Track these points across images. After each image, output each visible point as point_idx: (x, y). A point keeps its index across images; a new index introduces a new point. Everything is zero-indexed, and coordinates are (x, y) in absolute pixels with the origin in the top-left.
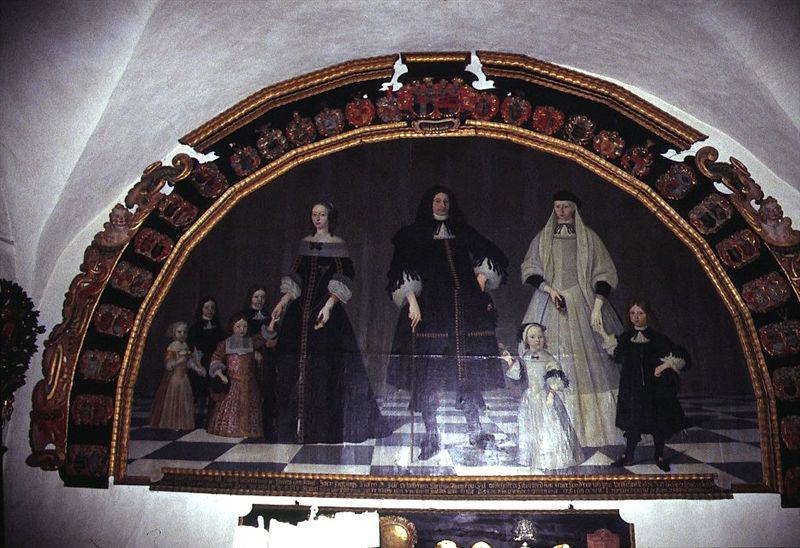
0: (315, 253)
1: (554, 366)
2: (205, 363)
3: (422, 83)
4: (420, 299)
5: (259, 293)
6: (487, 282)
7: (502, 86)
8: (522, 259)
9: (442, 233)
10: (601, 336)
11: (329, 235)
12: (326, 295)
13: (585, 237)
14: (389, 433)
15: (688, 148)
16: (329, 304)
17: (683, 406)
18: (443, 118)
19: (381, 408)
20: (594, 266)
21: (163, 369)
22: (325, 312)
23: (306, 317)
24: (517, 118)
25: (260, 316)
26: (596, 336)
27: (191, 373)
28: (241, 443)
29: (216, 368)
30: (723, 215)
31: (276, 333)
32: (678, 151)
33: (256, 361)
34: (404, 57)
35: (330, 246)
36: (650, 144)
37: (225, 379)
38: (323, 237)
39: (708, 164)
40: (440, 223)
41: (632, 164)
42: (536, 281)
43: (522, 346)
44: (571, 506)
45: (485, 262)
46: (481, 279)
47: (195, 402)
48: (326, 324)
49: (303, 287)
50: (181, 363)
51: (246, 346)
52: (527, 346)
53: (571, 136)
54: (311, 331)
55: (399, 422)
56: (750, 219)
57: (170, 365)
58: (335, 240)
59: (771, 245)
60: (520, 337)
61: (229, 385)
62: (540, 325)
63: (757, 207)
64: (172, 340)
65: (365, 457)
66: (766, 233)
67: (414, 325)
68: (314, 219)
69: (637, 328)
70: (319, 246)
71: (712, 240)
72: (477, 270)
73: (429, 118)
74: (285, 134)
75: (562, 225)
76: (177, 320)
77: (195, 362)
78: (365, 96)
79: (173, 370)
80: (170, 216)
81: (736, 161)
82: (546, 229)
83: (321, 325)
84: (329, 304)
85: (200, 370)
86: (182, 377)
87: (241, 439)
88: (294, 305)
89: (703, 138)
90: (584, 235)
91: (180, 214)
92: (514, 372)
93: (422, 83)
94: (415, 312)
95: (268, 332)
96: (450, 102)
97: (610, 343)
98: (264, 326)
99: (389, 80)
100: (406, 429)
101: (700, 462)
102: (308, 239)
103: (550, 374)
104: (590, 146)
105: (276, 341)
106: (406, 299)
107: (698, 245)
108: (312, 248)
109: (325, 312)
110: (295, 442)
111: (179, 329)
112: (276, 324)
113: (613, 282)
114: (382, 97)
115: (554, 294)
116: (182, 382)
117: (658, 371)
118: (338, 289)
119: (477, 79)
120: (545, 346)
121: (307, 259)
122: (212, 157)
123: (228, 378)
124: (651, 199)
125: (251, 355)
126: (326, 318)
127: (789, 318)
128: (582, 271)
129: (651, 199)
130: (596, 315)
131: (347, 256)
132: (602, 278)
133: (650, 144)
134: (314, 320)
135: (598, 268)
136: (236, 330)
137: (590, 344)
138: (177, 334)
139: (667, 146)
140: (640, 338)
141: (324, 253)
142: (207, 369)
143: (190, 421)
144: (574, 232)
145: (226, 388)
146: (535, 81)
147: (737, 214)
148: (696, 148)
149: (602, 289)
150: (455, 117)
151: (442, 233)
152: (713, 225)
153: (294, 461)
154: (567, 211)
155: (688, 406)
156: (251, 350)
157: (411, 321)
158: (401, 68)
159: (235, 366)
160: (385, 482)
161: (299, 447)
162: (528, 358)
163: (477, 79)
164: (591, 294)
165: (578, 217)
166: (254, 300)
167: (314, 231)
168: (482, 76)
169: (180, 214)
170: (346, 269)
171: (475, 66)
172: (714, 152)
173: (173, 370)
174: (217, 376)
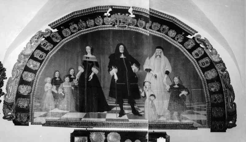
0: (88, 60)
1: (152, 93)
2: (57, 89)
3: (118, 14)
4: (117, 74)
5: (72, 70)
6: (135, 70)
7: (58, 28)
8: (143, 64)
9: (122, 56)
10: (165, 85)
11: (91, 55)
12: (91, 72)
13: (164, 59)
14: (110, 110)
15: (194, 35)
16: (92, 74)
17: (186, 104)
18: (123, 25)
19: (108, 103)
20: (165, 67)
21: (44, 91)
22: (91, 76)
23: (86, 77)
24: (142, 26)
25: (72, 77)
26: (164, 85)
27: (53, 93)
28: (69, 112)
29: (60, 91)
30: (201, 53)
31: (77, 82)
32: (191, 35)
33: (72, 89)
34: (111, 7)
35: (92, 58)
36: (183, 33)
37: (63, 94)
38: (89, 55)
39: (198, 39)
40: (121, 53)
41: (178, 39)
42: (149, 70)
43: (144, 87)
44: (154, 131)
45: (134, 64)
46: (133, 69)
47: (55, 100)
48: (92, 79)
49: (85, 69)
50: (49, 90)
51: (69, 85)
52: (146, 87)
53: (162, 31)
54: (87, 81)
55: (113, 107)
56: (208, 54)
57: (46, 90)
58: (93, 56)
59: (213, 62)
60: (144, 85)
61: (64, 96)
62: (149, 82)
63: (210, 51)
64: (46, 83)
65: (104, 116)
66: (212, 58)
67: (116, 81)
68: (87, 50)
69: (175, 83)
70: (89, 58)
71: (198, 60)
72: (132, 66)
73: (119, 24)
74: (78, 26)
75: (157, 55)
76: (48, 77)
77: (54, 89)
78: (100, 17)
79: (47, 91)
80: (45, 46)
81: (206, 39)
82: (153, 56)
83: (90, 80)
84: (92, 74)
85: (56, 92)
86: (50, 93)
87: (69, 111)
88: (82, 75)
89: (197, 32)
90: (163, 59)
91: (48, 46)
92: (143, 94)
93: (118, 14)
94: (116, 78)
95: (75, 82)
96: (126, 21)
97: (168, 87)
98: (74, 80)
99: (106, 12)
100: (115, 109)
101: (189, 119)
102: (86, 56)
103: (152, 95)
104: (167, 34)
105: (78, 84)
106: (113, 74)
107: (194, 61)
108: (86, 58)
109: (91, 76)
110: (84, 112)
111: (48, 80)
112: (77, 79)
113: (170, 70)
114: (105, 17)
115: (154, 74)
116: (50, 95)
117: (180, 95)
118: (95, 70)
119: (130, 14)
120: (150, 88)
121: (85, 61)
122: (56, 30)
123: (64, 93)
124: (182, 49)
125: (71, 88)
126: (92, 78)
127: (216, 81)
128: (162, 68)
129: (182, 49)
130: (165, 80)
131: (97, 61)
132: (167, 70)
133: (183, 33)
134: (88, 78)
135: (166, 67)
136: (66, 80)
137: (162, 87)
138: (48, 81)
139: (188, 34)
140: (176, 86)
141: (90, 60)
142: (58, 91)
143: (53, 106)
144: (161, 57)
145: (64, 97)
146: (153, 15)
147: (205, 53)
148: (196, 34)
149: (167, 73)
150: (126, 25)
151: (122, 56)
152: (198, 56)
153: (84, 117)
154: (160, 52)
155: (187, 104)
156: (71, 86)
157: (115, 79)
158: (110, 10)
159: (66, 90)
160: (110, 123)
161: (86, 113)
162: (146, 91)
163: (130, 14)
164: (164, 74)
165: (162, 53)
166: (71, 72)
167: (87, 54)
168: (132, 14)
169: (48, 46)
170: (97, 65)
171: (130, 11)
172: (199, 36)
173: (47, 91)
174: (61, 94)
